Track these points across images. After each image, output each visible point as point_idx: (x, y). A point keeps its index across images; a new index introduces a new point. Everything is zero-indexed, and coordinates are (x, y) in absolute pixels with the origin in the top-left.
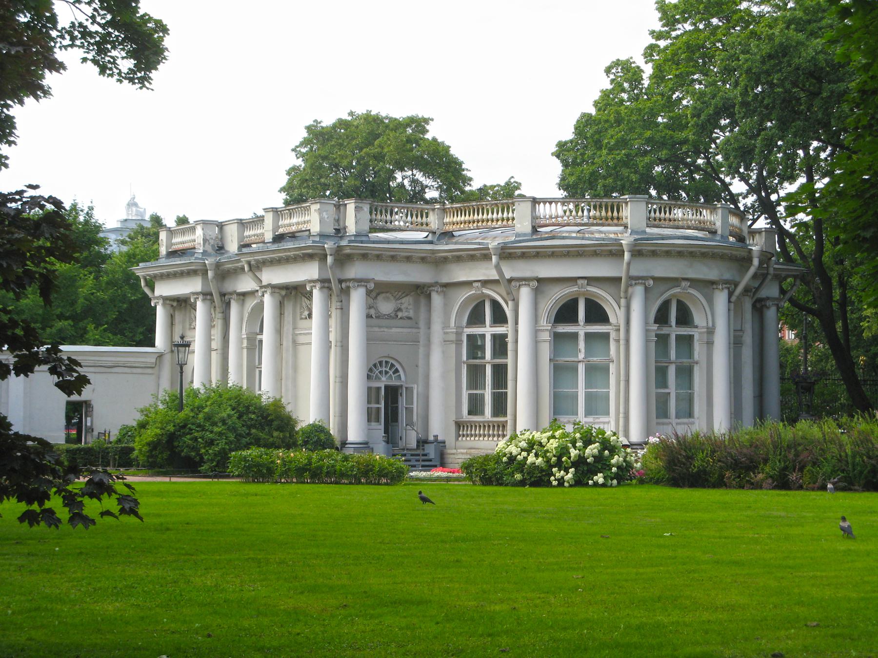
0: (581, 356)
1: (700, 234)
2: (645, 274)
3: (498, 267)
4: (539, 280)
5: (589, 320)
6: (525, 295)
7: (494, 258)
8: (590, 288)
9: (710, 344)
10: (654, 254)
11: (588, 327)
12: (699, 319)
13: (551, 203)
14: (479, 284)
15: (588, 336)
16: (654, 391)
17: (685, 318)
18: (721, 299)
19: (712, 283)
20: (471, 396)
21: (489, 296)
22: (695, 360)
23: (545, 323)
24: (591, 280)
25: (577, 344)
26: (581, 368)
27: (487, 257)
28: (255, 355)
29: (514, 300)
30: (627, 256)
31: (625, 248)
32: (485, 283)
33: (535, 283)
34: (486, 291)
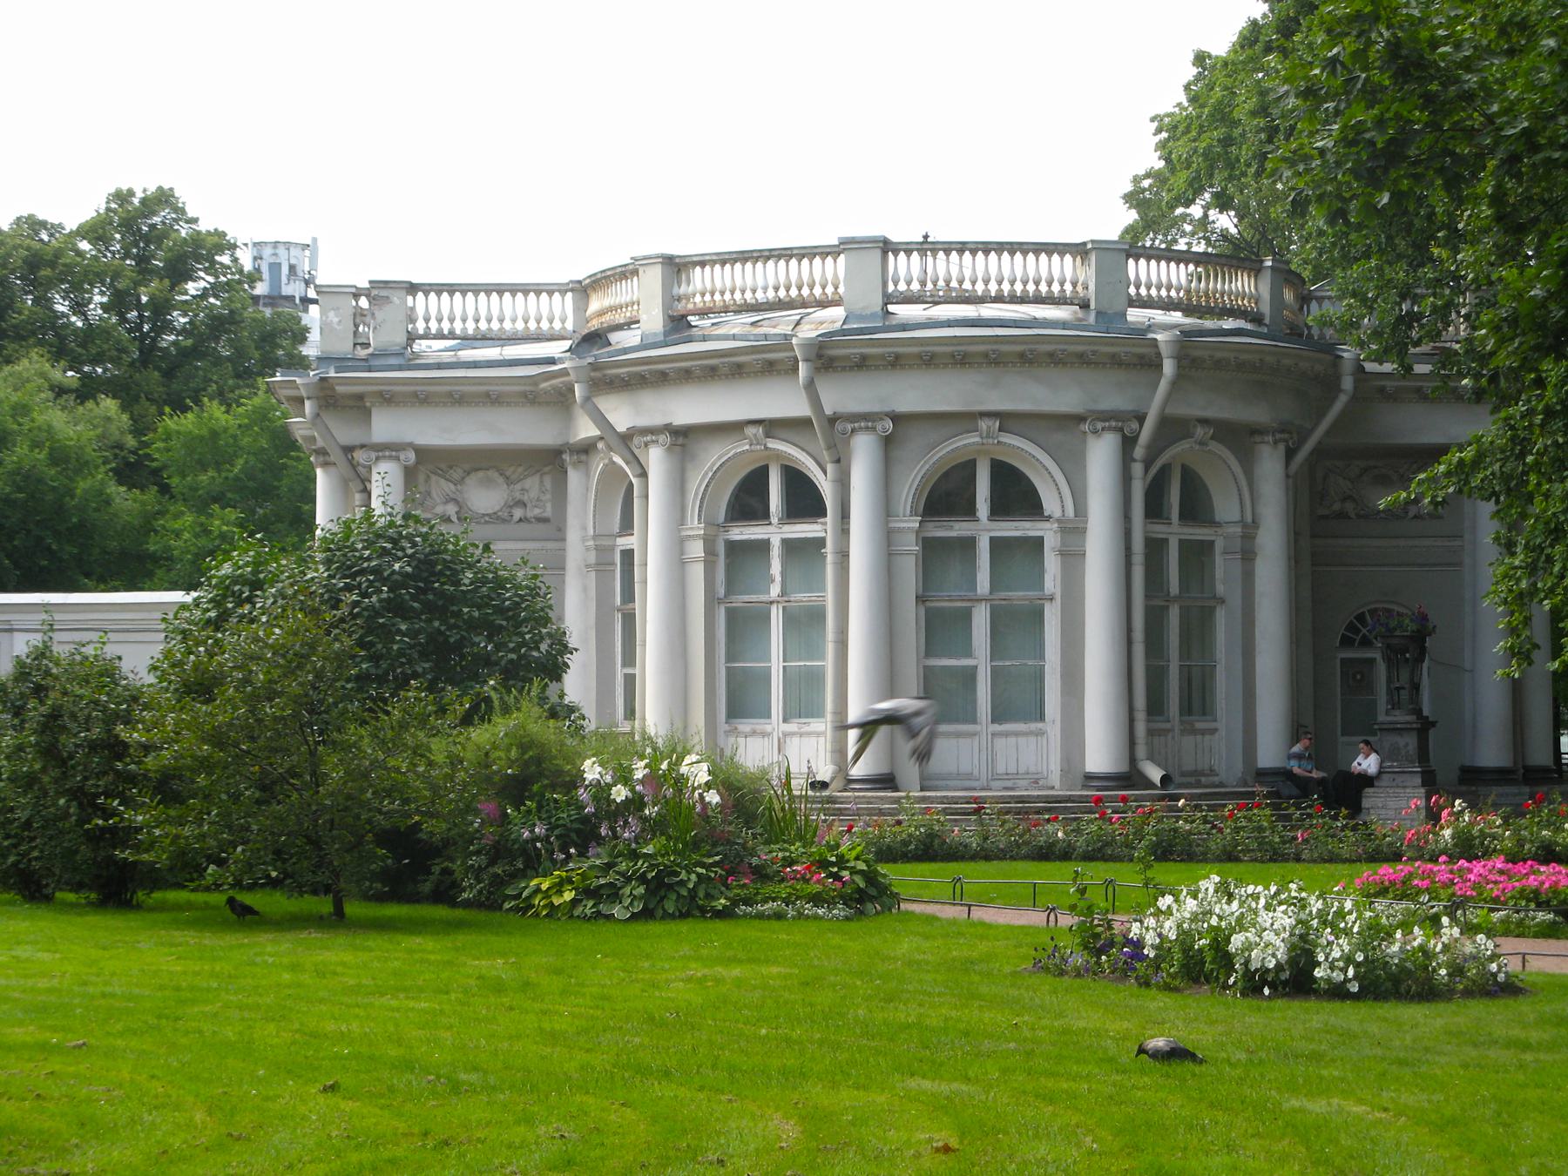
0: (775, 590)
1: (1240, 324)
2: (876, 408)
3: (810, 386)
4: (896, 418)
5: (1000, 509)
6: (656, 458)
9: (1248, 556)
10: (862, 364)
11: (787, 528)
12: (1226, 507)
13: (947, 252)
15: (996, 543)
16: (637, 671)
17: (1196, 507)
18: (1101, 455)
19: (1080, 419)
20: (728, 669)
21: (778, 455)
22: (1047, 592)
23: (695, 526)
24: (1007, 420)
25: (769, 566)
28: (614, 579)
29: (838, 461)
31: (1165, 350)
32: (772, 427)
33: (889, 425)
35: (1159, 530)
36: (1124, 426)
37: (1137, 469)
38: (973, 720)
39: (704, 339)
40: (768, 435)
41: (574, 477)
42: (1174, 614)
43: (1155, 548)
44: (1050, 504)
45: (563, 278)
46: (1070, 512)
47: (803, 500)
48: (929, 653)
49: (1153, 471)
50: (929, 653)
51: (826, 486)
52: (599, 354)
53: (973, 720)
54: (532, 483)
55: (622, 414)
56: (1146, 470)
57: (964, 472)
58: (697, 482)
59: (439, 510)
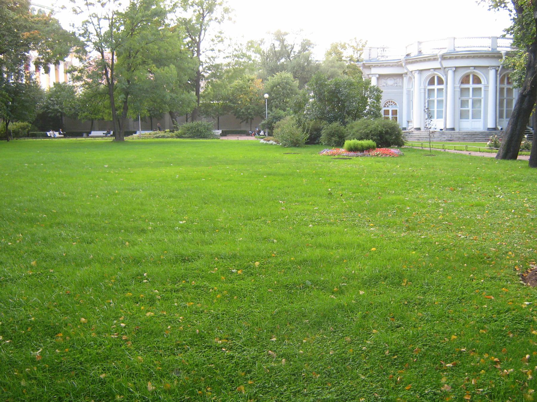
3: (441, 63)
4: (456, 68)
6: (450, 73)
7: (439, 59)
8: (475, 71)
10: (450, 58)
14: (433, 70)
15: (473, 89)
18: (492, 73)
19: (488, 67)
21: (436, 74)
23: (458, 85)
24: (475, 67)
26: (470, 102)
27: (435, 59)
30: (439, 59)
31: (503, 55)
32: (435, 69)
34: (436, 73)
35: (502, 86)
36: (496, 68)
37: (498, 76)
38: (468, 119)
39: (424, 55)
40: (434, 71)
41: (405, 78)
42: (505, 101)
43: (502, 90)
44: (483, 82)
45: (490, 36)
46: (486, 83)
47: (440, 82)
48: (461, 107)
49: (502, 76)
50: (461, 107)
51: (444, 79)
52: (408, 58)
53: (468, 119)
54: (398, 80)
55: (411, 67)
56: (500, 76)
57: (468, 76)
58: (423, 80)
59: (383, 84)
